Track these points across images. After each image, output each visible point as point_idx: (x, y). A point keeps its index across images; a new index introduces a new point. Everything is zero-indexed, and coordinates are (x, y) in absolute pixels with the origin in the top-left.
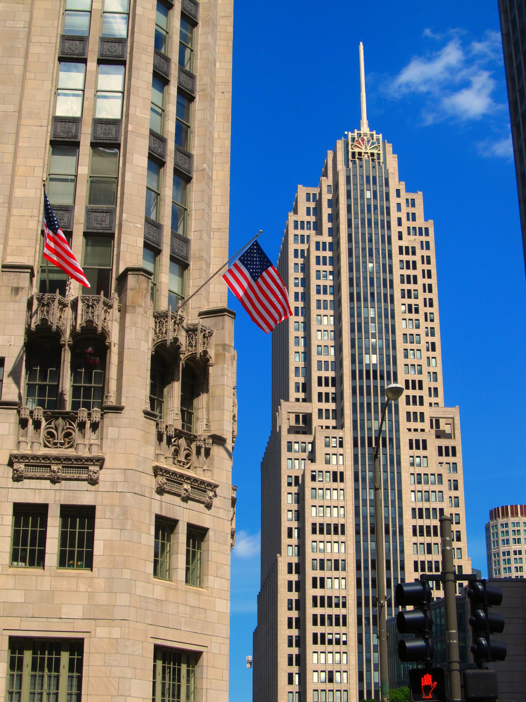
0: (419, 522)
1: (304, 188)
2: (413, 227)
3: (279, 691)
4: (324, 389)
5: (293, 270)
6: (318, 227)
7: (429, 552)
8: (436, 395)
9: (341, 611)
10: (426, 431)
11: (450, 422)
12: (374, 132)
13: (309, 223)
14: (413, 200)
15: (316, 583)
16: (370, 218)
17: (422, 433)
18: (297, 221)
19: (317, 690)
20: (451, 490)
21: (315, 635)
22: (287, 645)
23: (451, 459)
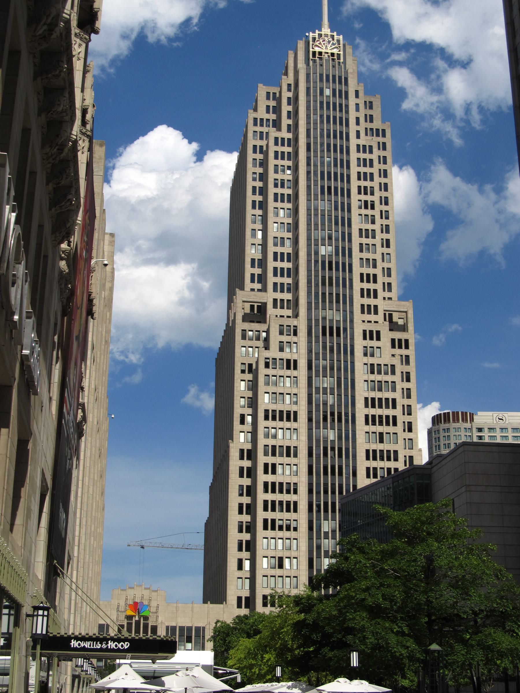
0: (372, 411)
1: (264, 87)
2: (370, 129)
3: (228, 576)
4: (279, 280)
5: (251, 165)
6: (277, 124)
7: (381, 441)
8: (390, 290)
9: (292, 498)
10: (379, 322)
11: (403, 317)
12: (335, 34)
13: (268, 120)
14: (371, 103)
15: (268, 469)
16: (329, 114)
17: (376, 324)
18: (257, 119)
19: (267, 576)
20: (404, 398)
21: (265, 521)
22: (237, 530)
23: (404, 352)
